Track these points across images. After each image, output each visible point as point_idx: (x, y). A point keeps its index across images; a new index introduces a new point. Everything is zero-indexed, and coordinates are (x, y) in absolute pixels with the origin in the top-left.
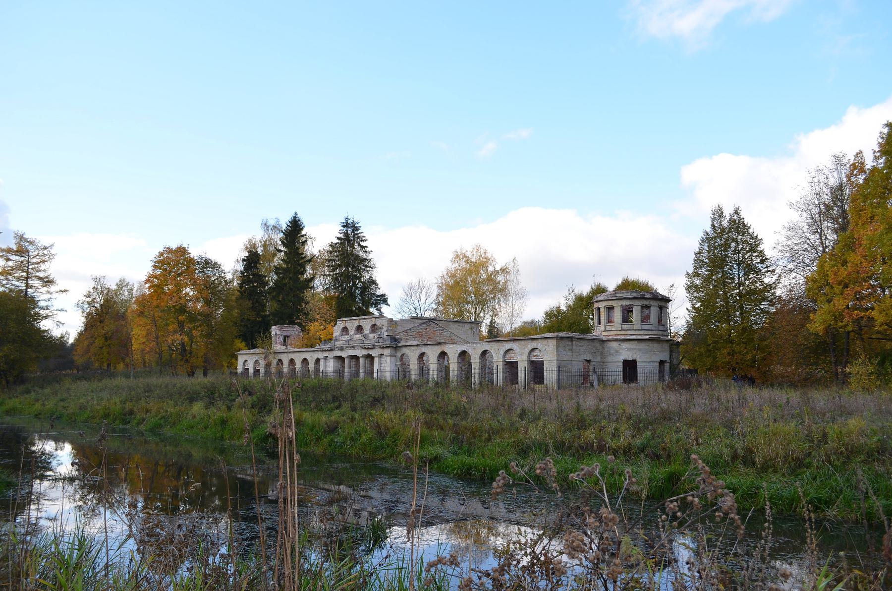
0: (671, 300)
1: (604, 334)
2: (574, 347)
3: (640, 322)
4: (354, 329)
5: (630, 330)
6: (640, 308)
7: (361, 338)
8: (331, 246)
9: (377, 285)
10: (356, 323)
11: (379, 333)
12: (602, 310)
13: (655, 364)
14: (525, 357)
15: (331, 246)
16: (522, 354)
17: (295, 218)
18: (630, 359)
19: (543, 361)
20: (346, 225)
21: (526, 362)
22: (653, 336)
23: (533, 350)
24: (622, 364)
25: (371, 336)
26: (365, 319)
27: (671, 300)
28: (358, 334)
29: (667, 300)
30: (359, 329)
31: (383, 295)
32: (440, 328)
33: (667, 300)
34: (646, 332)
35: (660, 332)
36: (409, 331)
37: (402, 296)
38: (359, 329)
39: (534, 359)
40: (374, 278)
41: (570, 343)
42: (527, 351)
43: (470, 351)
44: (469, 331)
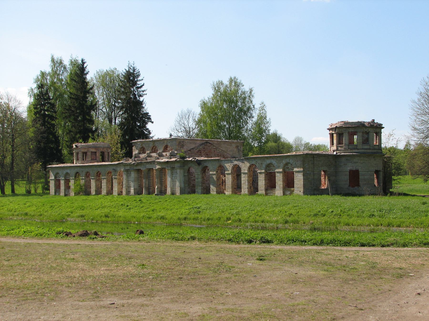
3: (361, 144)
5: (354, 149)
12: (335, 135)
18: (354, 169)
23: (287, 164)
24: (348, 173)
36: (192, 150)
39: (287, 170)
42: (282, 165)
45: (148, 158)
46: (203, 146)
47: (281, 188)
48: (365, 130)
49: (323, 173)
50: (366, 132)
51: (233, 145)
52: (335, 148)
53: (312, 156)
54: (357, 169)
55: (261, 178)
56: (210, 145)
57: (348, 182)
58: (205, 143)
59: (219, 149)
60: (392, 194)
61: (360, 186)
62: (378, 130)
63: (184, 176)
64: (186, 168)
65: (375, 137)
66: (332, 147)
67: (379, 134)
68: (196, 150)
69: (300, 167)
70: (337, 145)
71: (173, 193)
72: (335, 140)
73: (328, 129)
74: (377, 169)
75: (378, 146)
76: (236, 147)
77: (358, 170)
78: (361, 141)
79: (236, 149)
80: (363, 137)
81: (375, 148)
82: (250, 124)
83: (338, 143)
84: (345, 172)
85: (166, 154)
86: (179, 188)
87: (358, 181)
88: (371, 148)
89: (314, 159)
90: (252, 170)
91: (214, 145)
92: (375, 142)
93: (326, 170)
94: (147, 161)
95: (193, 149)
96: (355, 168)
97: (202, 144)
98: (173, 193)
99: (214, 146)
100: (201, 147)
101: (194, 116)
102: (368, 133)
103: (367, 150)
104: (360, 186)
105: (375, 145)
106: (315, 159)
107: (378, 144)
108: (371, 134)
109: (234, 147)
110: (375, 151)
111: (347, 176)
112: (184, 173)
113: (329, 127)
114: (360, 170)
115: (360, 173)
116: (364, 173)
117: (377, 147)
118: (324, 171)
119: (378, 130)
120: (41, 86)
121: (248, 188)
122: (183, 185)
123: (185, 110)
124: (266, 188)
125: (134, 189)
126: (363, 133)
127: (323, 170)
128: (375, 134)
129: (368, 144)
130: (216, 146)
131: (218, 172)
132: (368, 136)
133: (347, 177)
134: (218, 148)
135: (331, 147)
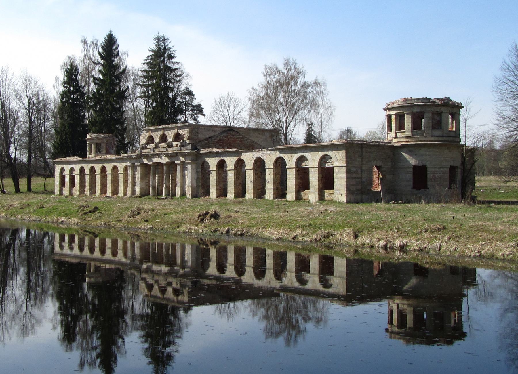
0: (463, 107)
1: (395, 140)
2: (364, 154)
3: (431, 128)
4: (159, 137)
6: (430, 115)
7: (165, 146)
8: (132, 68)
9: (193, 95)
10: (160, 133)
11: (181, 141)
12: (393, 117)
13: (446, 170)
14: (316, 164)
15: (132, 68)
16: (313, 160)
17: (71, 65)
19: (333, 168)
20: (158, 39)
21: (69, 176)
22: (404, 143)
24: (411, 170)
25: (174, 144)
26: (434, 131)
27: (463, 107)
28: (162, 142)
29: (459, 106)
30: (164, 138)
31: (199, 106)
32: (240, 137)
33: (459, 106)
34: (436, 139)
35: (452, 138)
36: (210, 140)
37: (213, 105)
38: (164, 138)
40: (190, 89)
41: (360, 150)
43: (265, 158)
44: (269, 140)
45: (156, 150)
46: (225, 134)
47: (317, 190)
48: (438, 110)
49: (375, 169)
50: (438, 112)
51: (266, 134)
52: (393, 134)
53: (360, 145)
54: (424, 165)
55: (290, 176)
56: (234, 133)
57: (411, 183)
58: (228, 130)
59: (247, 139)
60: (474, 200)
61: (428, 188)
62: (454, 110)
63: (197, 172)
64: (200, 161)
65: (450, 120)
66: (390, 134)
67: (456, 116)
68: (215, 139)
69: (171, 253)
70: (396, 131)
71: (183, 194)
72: (393, 124)
73: (385, 110)
74: (452, 165)
75: (455, 132)
76: (270, 136)
77: (426, 166)
78: (431, 125)
79: (271, 140)
80: (432, 119)
81: (452, 135)
82: (114, 47)
83: (397, 128)
84: (406, 168)
85: (177, 145)
86: (190, 188)
87: (426, 181)
88: (445, 135)
89: (362, 150)
90: (279, 165)
91: (241, 133)
92: (450, 127)
93: (380, 165)
94: (288, 146)
95: (211, 137)
96: (422, 162)
97: (225, 132)
98: (183, 194)
99: (240, 135)
100: (222, 136)
101: (236, 104)
102: (440, 114)
103: (439, 137)
104: (428, 188)
105: (450, 131)
106: (364, 149)
107: (454, 129)
108: (444, 115)
109: (268, 136)
110: (451, 139)
111: (410, 173)
112: (197, 168)
113: (384, 107)
114: (428, 166)
115: (428, 169)
116: (433, 170)
117: (453, 134)
118: (377, 167)
119: (454, 110)
120: (67, 72)
121: (274, 189)
122: (195, 184)
123: (225, 94)
124: (297, 189)
125: (140, 188)
126: (433, 114)
127: (375, 166)
128: (450, 116)
129: (441, 129)
130: (243, 135)
131: (237, 167)
132: (441, 118)
133: (410, 176)
134: (246, 137)
135: (388, 134)
